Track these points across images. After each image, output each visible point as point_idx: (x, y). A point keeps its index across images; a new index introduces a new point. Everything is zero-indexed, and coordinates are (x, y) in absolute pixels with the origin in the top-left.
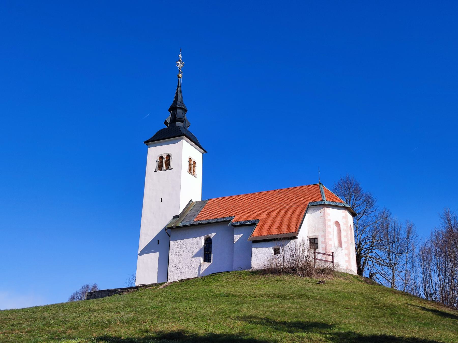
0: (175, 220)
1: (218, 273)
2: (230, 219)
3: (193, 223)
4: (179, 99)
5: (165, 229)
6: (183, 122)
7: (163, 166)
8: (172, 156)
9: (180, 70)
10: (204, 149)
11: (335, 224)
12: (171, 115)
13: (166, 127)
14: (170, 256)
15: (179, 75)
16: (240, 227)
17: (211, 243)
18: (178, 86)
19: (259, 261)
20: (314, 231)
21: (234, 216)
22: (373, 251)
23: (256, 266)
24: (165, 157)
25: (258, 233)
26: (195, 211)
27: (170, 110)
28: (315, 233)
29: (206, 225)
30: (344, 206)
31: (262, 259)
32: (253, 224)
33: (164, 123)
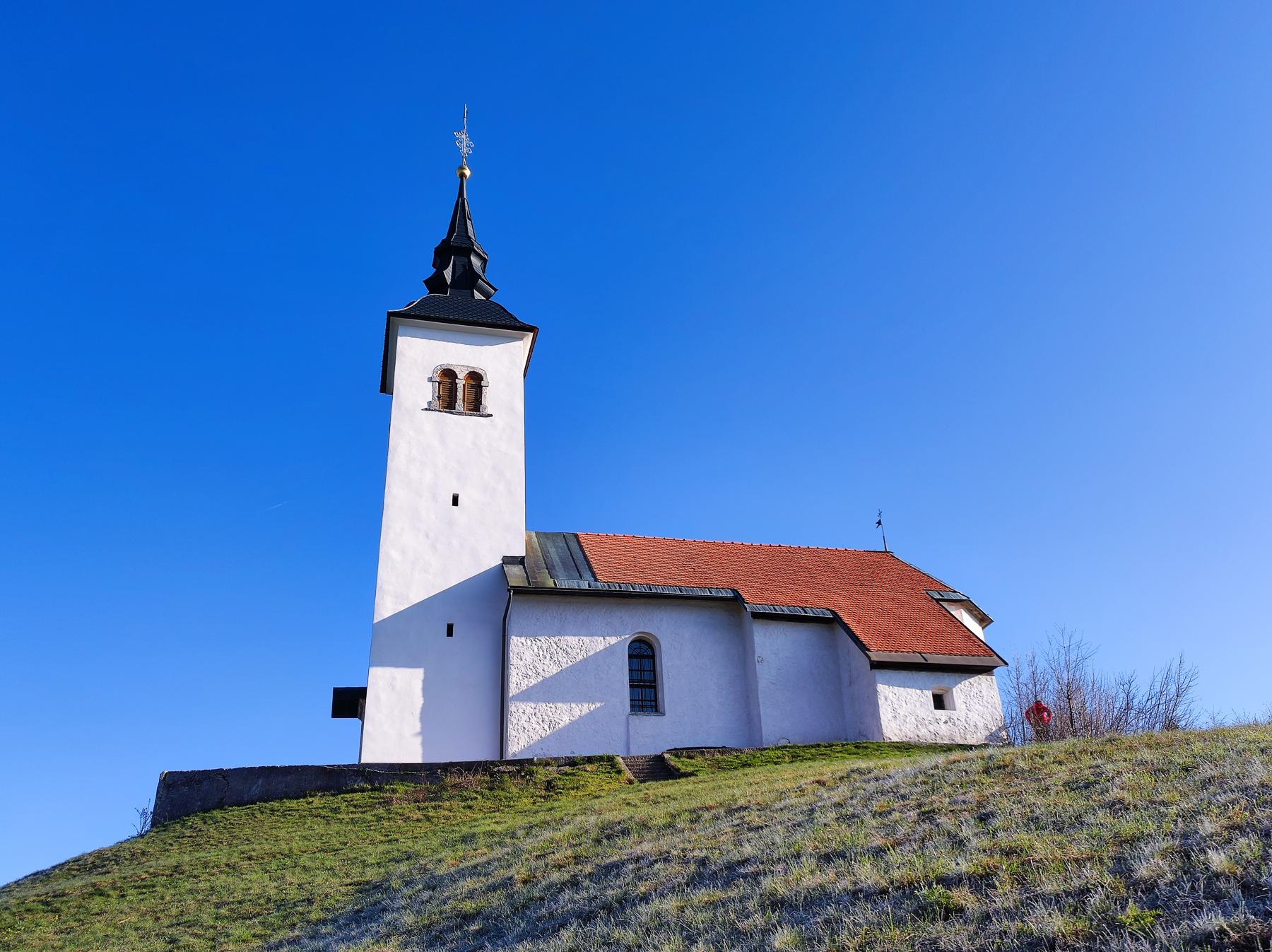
1: (702, 748)
15: (462, 168)
24: (462, 375)
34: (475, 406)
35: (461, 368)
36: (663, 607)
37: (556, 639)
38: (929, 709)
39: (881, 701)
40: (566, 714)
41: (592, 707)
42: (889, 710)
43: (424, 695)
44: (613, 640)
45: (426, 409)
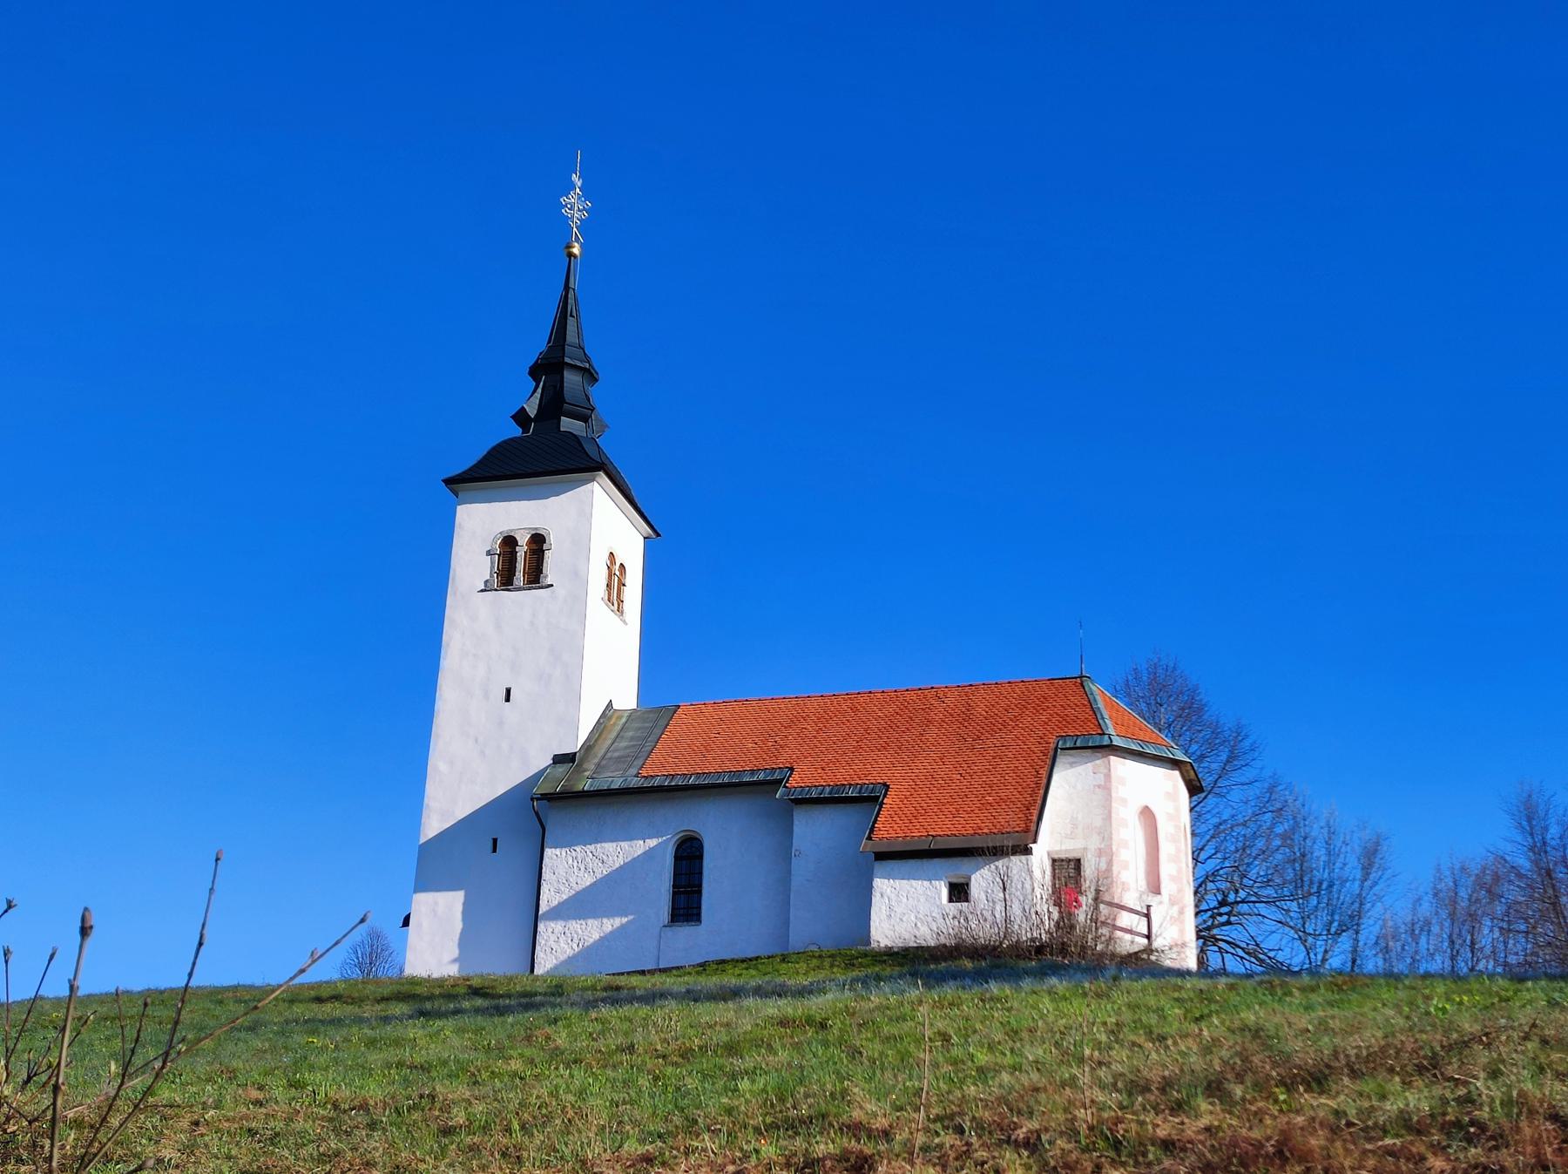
0: (561, 769)
2: (777, 776)
3: (634, 782)
4: (571, 336)
5: (532, 799)
6: (585, 419)
7: (517, 574)
8: (553, 540)
9: (575, 229)
10: (648, 517)
11: (1139, 817)
12: (542, 395)
13: (517, 431)
14: (545, 896)
15: (569, 246)
16: (815, 806)
17: (701, 857)
18: (567, 287)
19: (898, 920)
20: (1072, 833)
21: (789, 766)
22: (1233, 919)
23: (887, 937)
24: (523, 540)
25: (890, 827)
26: (632, 743)
27: (535, 372)
28: (1072, 841)
29: (679, 794)
30: (1172, 757)
31: (907, 916)
32: (870, 799)
33: (513, 417)
34: (535, 577)
35: (522, 531)
36: (712, 798)
37: (592, 847)
38: (935, 903)
39: (876, 899)
40: (593, 930)
41: (625, 920)
42: (884, 907)
43: (464, 919)
44: (652, 843)
45: (482, 591)
